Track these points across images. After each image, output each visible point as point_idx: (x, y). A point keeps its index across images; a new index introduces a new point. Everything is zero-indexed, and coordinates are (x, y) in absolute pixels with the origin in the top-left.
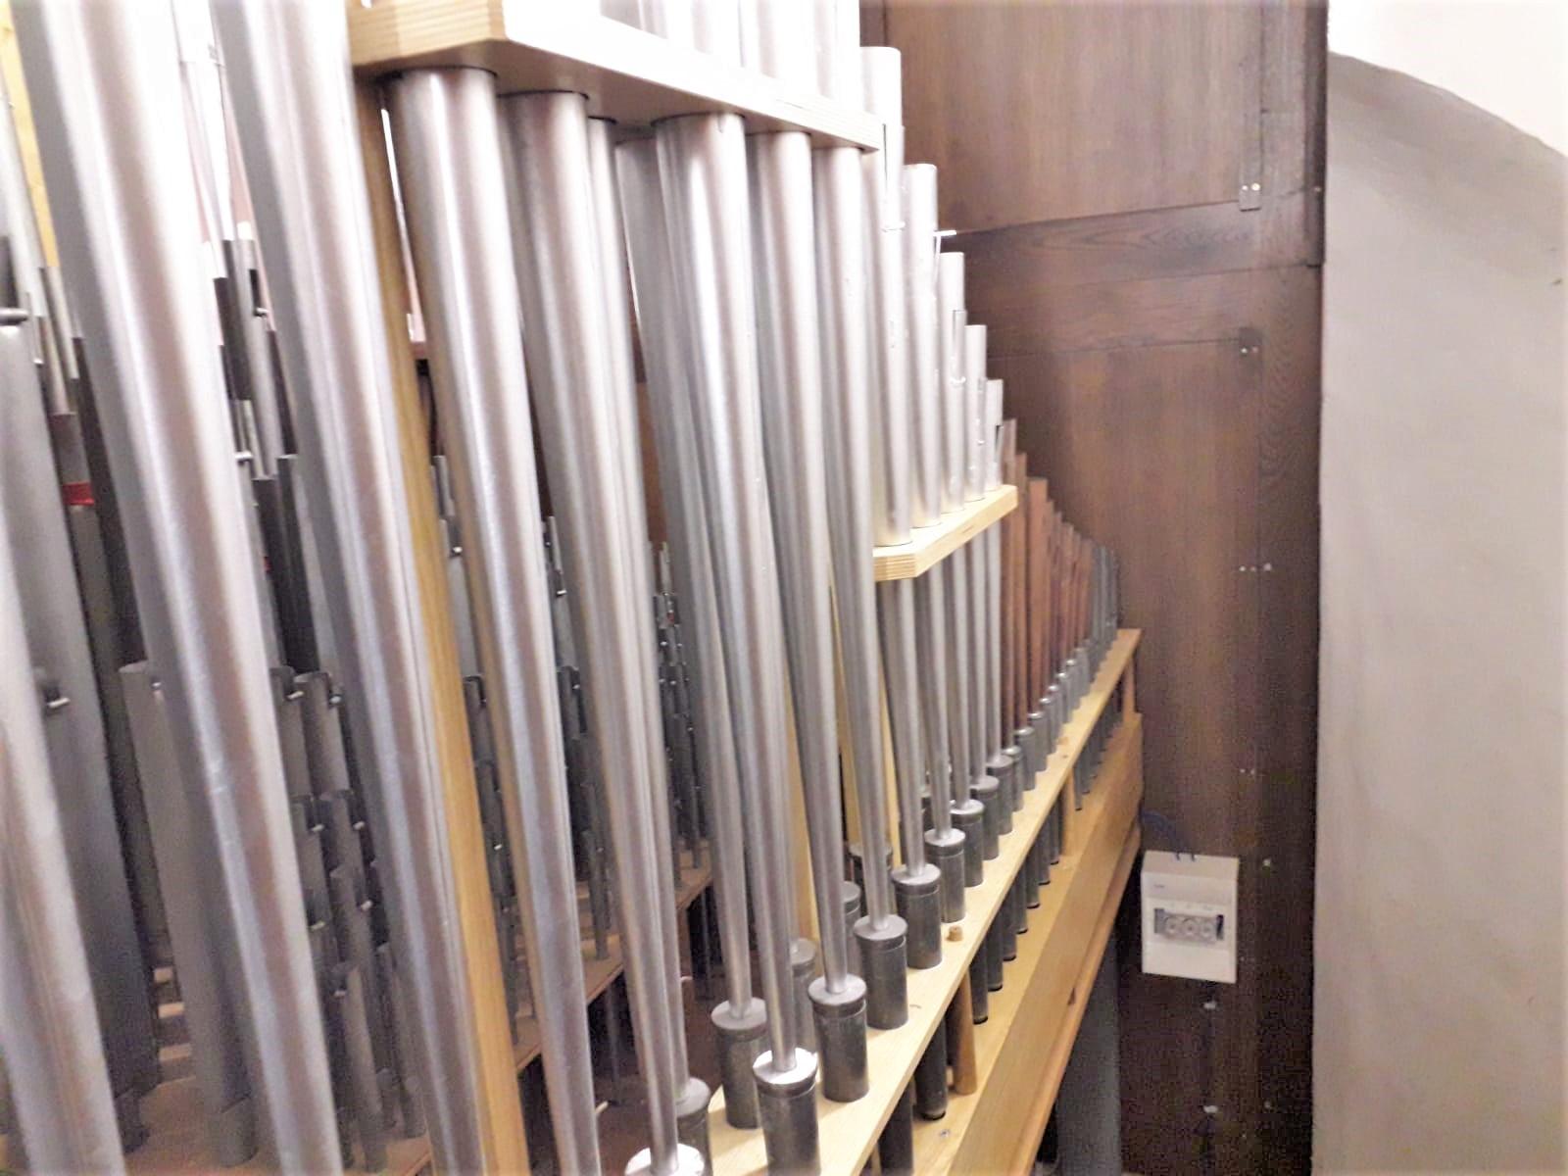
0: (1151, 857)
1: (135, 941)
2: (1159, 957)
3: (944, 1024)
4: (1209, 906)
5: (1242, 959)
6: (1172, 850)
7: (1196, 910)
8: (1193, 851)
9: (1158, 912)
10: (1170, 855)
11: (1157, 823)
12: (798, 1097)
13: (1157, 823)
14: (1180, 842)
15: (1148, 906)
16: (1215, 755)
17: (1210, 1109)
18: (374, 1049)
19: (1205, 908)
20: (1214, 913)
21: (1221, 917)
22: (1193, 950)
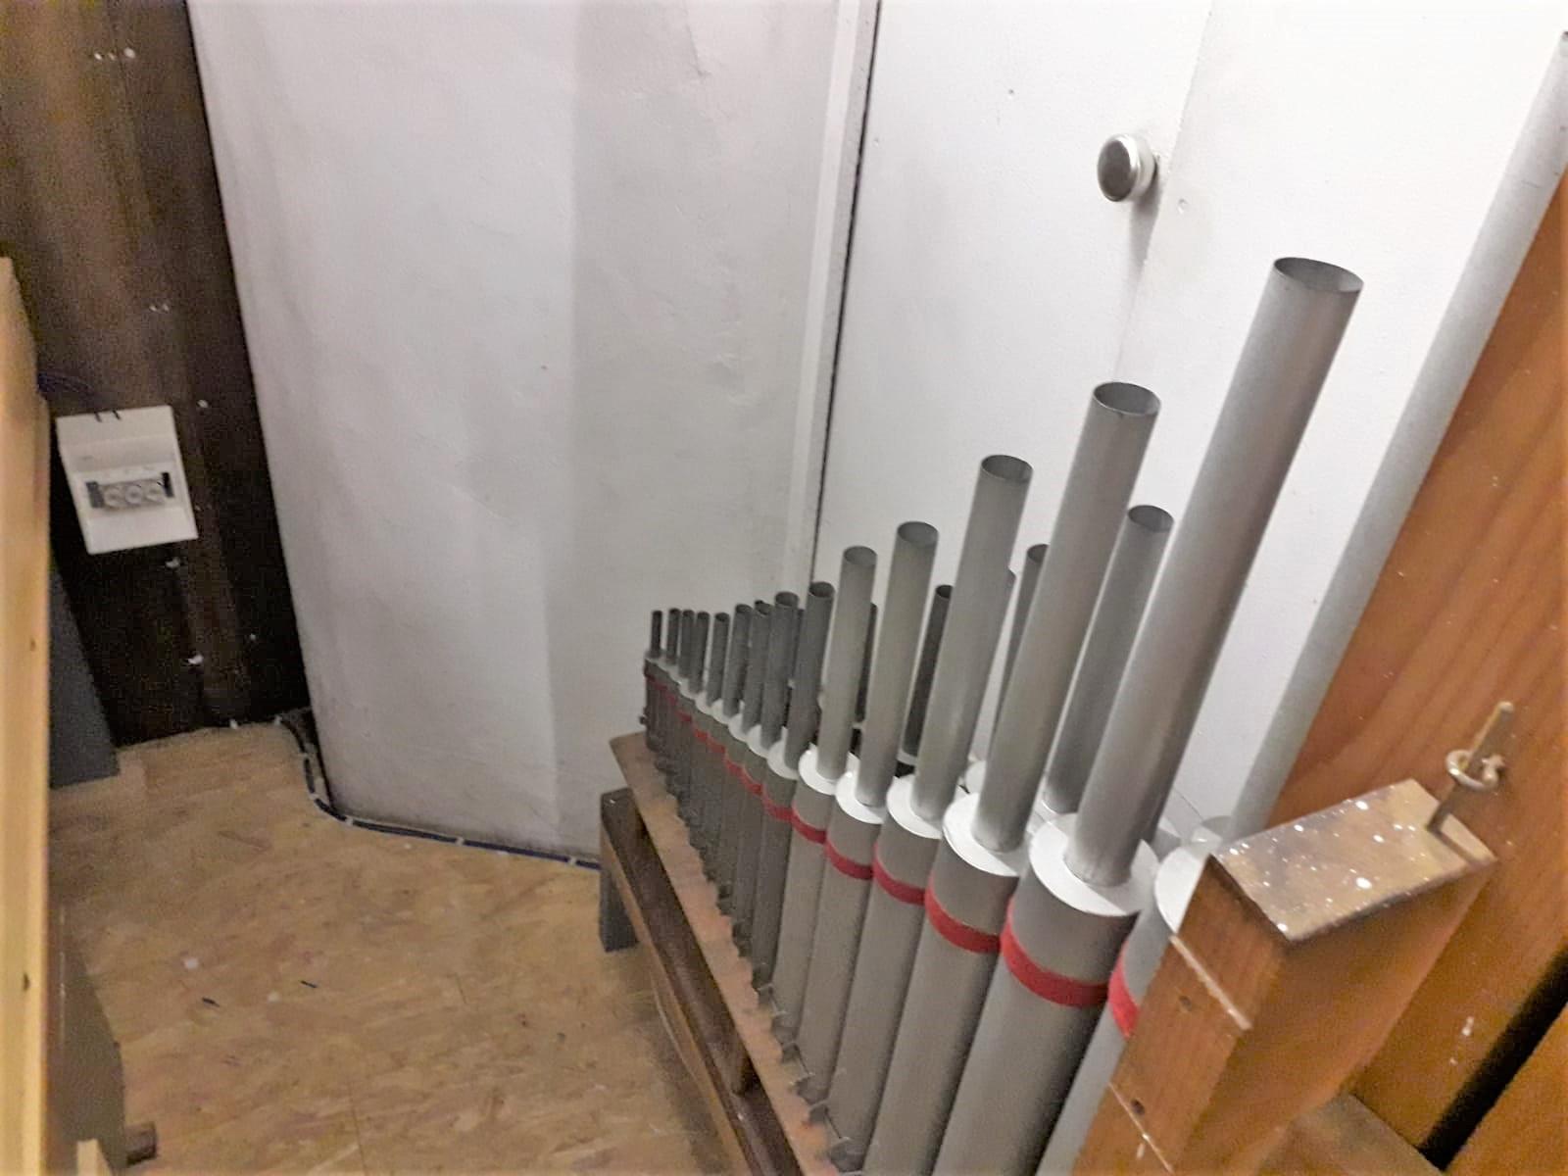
0: (64, 424)
1: (839, 1063)
2: (103, 534)
3: (607, 838)
4: (148, 466)
5: (198, 508)
6: (88, 411)
7: (138, 473)
8: (114, 408)
9: (92, 487)
10: (89, 418)
11: (64, 384)
12: (977, 773)
13: (64, 384)
14: (93, 402)
15: (77, 483)
16: (121, 308)
17: (196, 660)
18: (911, 712)
19: (147, 469)
20: (156, 473)
21: (166, 477)
22: (148, 516)
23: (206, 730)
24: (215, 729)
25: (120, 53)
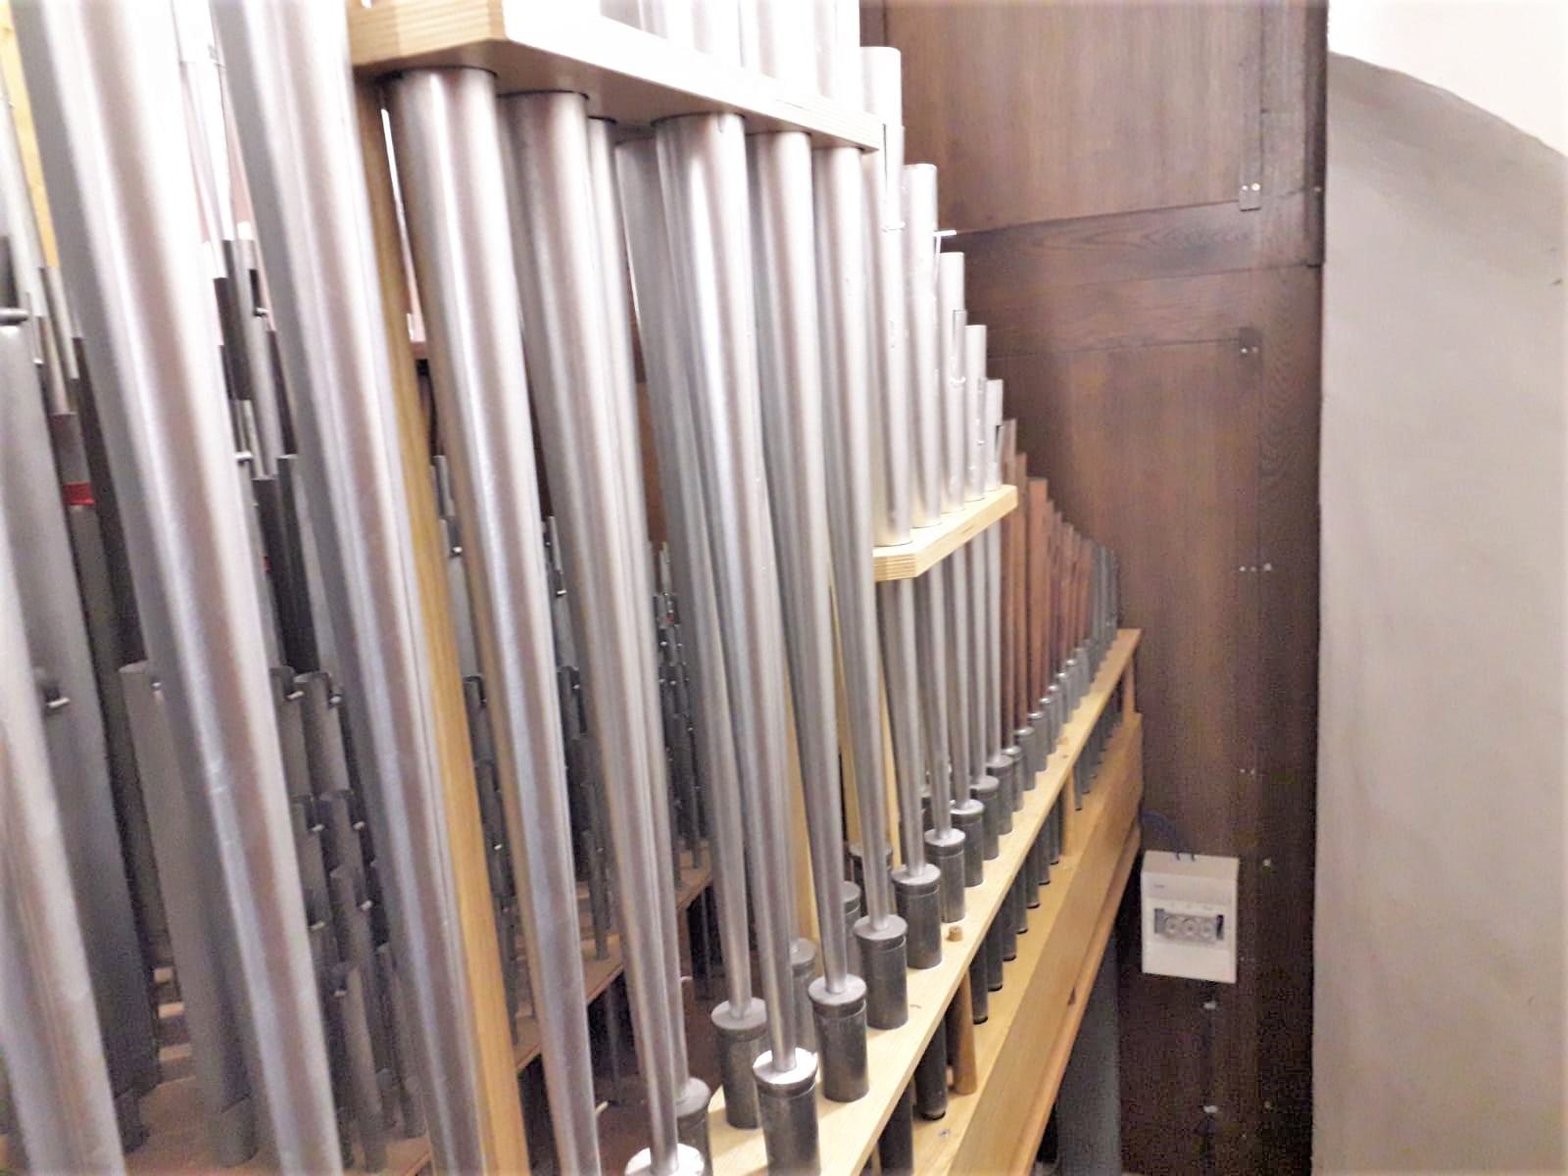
0: (1151, 857)
2: (1159, 957)
3: (944, 1024)
4: (1209, 906)
5: (1242, 959)
6: (1171, 850)
7: (1196, 910)
8: (1193, 851)
9: (1158, 912)
10: (1170, 855)
11: (1157, 823)
13: (1157, 823)
14: (1180, 842)
15: (1148, 906)
16: (1215, 755)
17: (1210, 1109)
18: (374, 1049)
19: (1205, 908)
20: (1214, 913)
21: (1221, 917)
23: (27, 1152)
24: (1313, 1126)
25: (1259, 567)
